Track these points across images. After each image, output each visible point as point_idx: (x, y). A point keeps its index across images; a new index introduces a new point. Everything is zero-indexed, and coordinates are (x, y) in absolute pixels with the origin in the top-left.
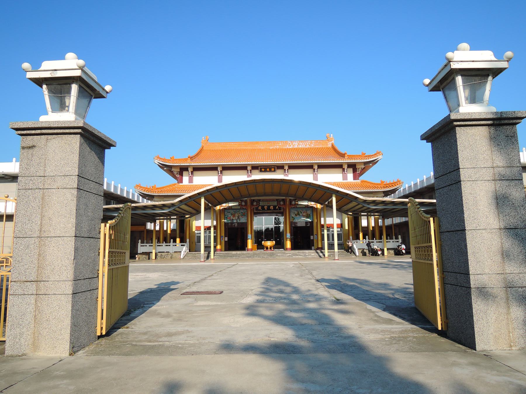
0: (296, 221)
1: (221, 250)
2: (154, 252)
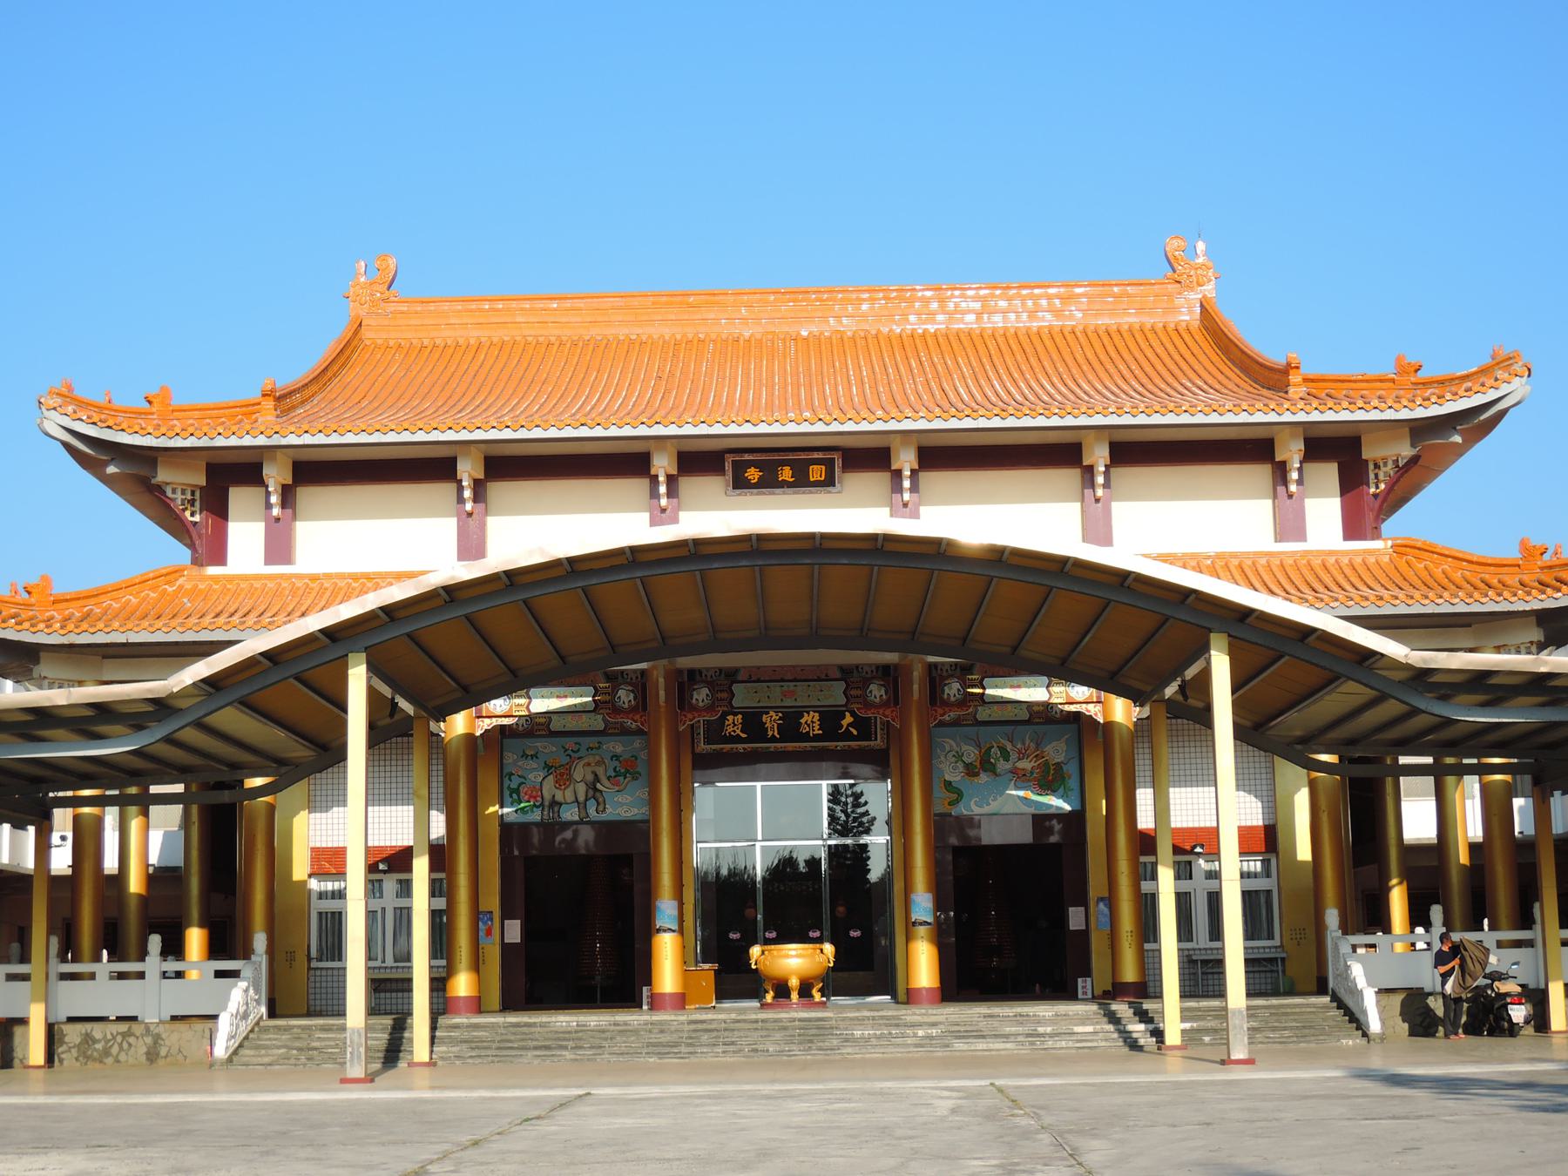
2: (37, 1016)
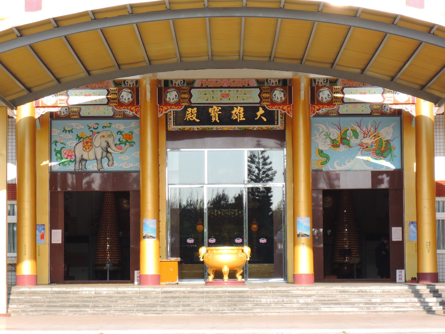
0: (334, 166)
1: (35, 280)
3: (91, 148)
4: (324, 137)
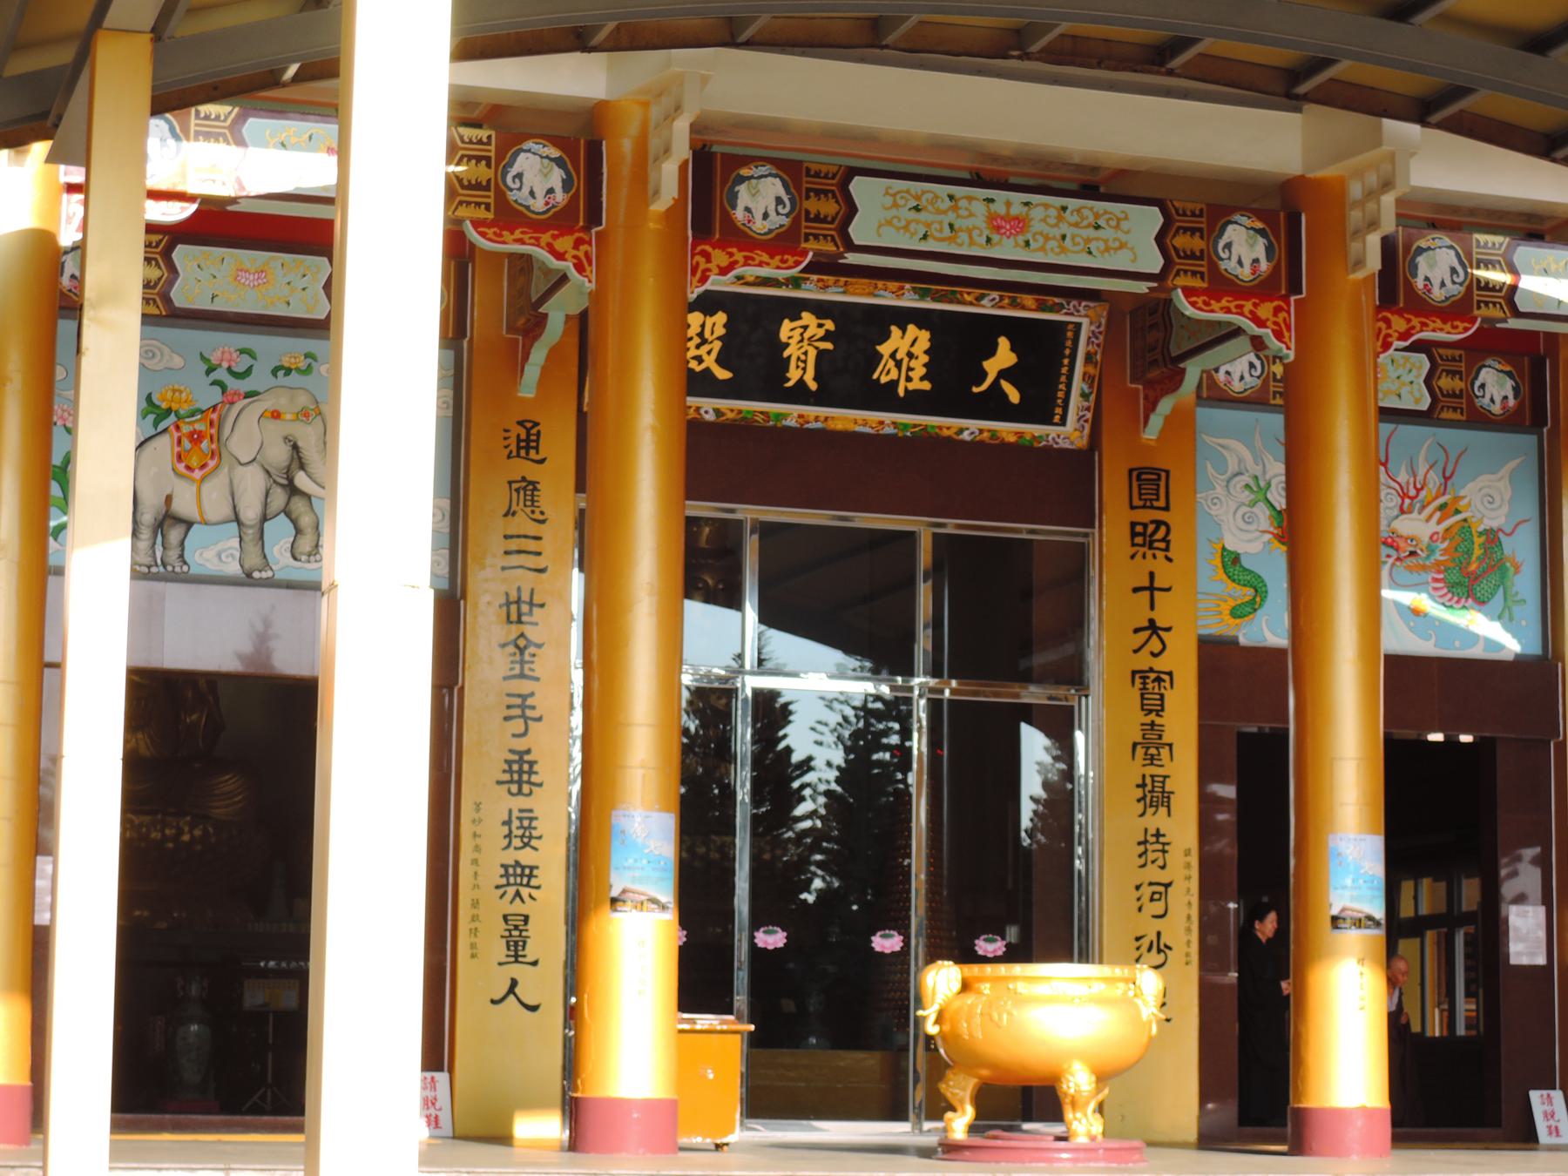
3: (212, 464)
4: (1246, 496)
